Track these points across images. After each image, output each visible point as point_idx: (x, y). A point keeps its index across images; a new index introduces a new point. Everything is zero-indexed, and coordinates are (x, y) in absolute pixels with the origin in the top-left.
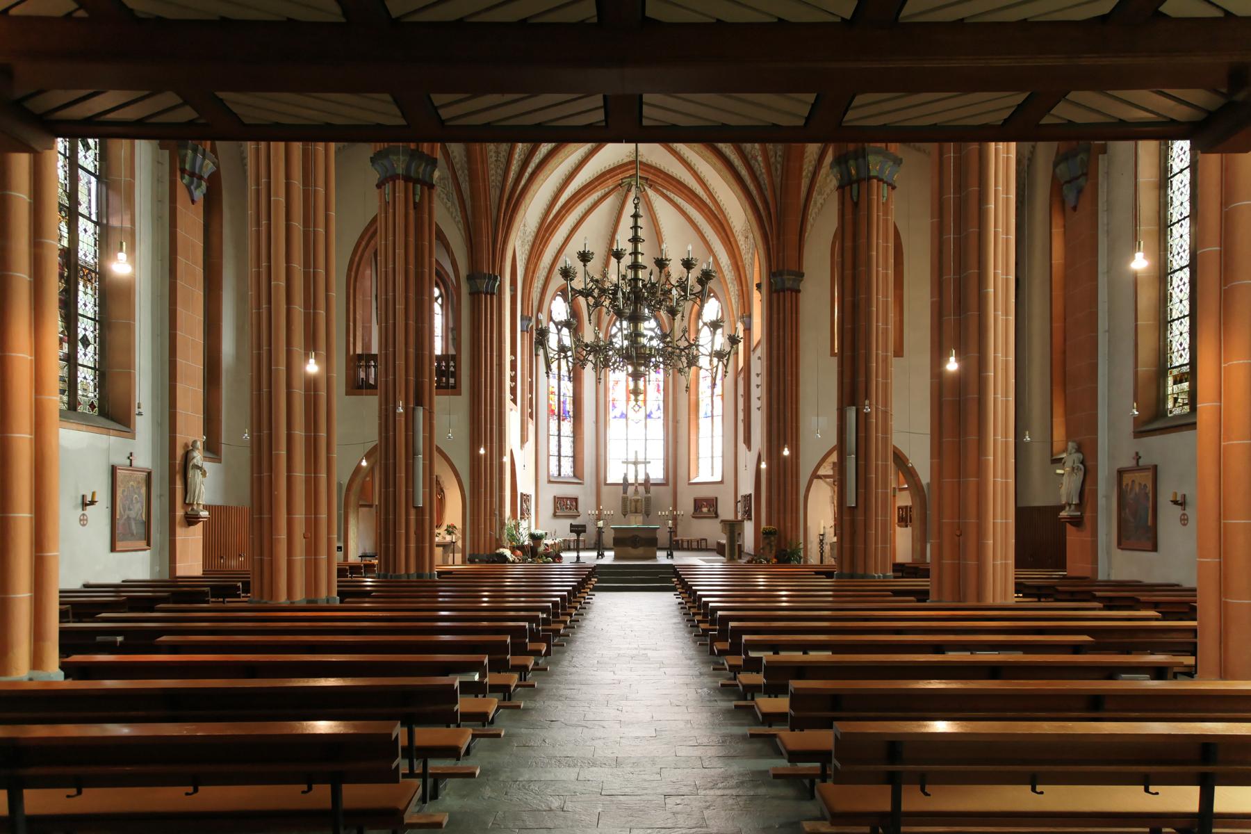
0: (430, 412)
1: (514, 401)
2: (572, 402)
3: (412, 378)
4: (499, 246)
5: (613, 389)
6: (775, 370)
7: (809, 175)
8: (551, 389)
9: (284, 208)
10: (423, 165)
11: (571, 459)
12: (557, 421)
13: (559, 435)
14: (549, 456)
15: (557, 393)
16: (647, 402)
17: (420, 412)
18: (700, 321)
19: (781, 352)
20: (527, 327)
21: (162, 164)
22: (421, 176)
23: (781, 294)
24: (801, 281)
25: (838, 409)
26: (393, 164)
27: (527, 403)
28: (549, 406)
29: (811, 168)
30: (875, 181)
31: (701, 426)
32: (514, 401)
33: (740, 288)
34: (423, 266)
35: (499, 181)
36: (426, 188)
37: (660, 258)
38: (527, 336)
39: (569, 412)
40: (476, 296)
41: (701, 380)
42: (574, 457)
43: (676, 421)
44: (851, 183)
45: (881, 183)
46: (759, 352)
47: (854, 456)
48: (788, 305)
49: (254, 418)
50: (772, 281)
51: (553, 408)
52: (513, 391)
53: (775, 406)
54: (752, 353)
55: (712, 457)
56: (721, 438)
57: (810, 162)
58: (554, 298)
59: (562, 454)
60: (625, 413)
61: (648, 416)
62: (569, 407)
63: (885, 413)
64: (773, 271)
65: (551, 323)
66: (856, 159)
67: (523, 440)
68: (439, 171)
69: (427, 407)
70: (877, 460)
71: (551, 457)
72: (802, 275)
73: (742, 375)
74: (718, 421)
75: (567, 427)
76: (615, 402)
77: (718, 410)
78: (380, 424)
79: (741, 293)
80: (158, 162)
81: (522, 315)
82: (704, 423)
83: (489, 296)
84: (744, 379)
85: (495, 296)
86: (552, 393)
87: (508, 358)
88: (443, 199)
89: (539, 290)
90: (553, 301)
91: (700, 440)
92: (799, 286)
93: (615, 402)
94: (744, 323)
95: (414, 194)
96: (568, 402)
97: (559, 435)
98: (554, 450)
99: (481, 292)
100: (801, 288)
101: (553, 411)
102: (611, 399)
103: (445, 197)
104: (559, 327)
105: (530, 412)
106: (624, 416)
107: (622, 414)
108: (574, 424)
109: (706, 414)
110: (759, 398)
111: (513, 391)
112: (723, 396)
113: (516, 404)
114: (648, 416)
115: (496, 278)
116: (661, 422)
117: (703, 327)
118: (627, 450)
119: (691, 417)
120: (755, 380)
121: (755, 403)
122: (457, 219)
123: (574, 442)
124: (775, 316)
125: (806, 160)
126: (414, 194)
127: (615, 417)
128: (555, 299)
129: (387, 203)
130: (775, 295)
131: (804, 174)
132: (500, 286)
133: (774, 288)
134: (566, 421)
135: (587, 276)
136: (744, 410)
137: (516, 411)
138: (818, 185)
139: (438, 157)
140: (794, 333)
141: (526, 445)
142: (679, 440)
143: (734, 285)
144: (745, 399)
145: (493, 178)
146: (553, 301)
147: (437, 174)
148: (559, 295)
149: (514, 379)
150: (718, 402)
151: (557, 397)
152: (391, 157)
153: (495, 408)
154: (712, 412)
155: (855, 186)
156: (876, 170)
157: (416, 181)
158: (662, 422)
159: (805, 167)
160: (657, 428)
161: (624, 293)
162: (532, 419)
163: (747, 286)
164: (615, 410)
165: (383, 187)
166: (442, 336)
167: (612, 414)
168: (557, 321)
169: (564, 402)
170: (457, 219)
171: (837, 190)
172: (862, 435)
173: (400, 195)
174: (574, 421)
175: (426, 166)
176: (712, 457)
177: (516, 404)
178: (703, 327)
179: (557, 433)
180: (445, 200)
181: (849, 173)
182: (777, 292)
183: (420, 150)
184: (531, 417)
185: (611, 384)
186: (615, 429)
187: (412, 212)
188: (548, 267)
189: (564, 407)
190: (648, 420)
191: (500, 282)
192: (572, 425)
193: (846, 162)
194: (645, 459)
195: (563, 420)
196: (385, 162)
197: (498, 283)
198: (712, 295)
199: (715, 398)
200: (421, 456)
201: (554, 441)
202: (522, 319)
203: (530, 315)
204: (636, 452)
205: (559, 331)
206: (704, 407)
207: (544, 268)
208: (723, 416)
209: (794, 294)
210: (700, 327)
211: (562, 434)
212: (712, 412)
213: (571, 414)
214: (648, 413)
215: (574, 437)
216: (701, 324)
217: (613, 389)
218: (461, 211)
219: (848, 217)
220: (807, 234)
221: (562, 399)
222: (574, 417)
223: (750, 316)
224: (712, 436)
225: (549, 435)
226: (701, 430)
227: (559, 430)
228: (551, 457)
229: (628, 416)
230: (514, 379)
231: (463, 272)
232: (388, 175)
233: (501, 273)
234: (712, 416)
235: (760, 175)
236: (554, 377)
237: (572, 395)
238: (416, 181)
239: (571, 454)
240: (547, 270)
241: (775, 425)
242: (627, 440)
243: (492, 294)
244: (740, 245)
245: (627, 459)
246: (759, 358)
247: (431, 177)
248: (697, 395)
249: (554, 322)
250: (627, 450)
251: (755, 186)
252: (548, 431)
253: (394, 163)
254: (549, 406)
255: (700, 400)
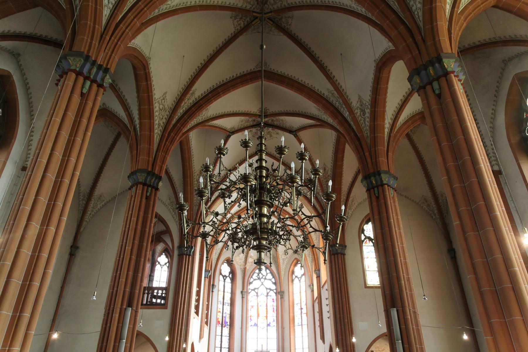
0: (136, 311)
1: (197, 313)
2: (229, 317)
3: (128, 290)
4: (195, 232)
5: (251, 310)
6: (336, 296)
7: (344, 201)
8: (219, 310)
9: (44, 166)
10: (154, 179)
11: (227, 349)
12: (221, 327)
13: (222, 336)
14: (215, 347)
15: (222, 312)
16: (268, 318)
17: (129, 311)
18: (294, 275)
19: (339, 285)
20: (208, 275)
21: (20, 177)
22: (152, 184)
23: (336, 255)
24: (345, 249)
25: (384, 310)
26: (138, 178)
27: (204, 316)
28: (217, 319)
29: (345, 198)
30: (386, 186)
31: (296, 330)
32: (197, 313)
33: (313, 256)
34: (145, 228)
35: (198, 203)
36: (154, 190)
37: (280, 145)
38: (207, 280)
39: (227, 322)
40: (181, 256)
41: (295, 305)
42: (229, 348)
43: (283, 328)
44: (373, 188)
45: (389, 187)
46: (326, 287)
47: (400, 341)
48: (340, 261)
49: (102, 336)
50: (331, 249)
51: (219, 320)
52: (197, 307)
53: (338, 316)
54: (321, 289)
55: (303, 348)
56: (307, 337)
57: (344, 195)
58: (223, 264)
59: (222, 347)
60: (256, 323)
61: (268, 325)
62: (228, 320)
63: (415, 312)
64: (331, 244)
65: (221, 276)
66: (375, 176)
67: (201, 337)
68: (162, 182)
69: (134, 308)
70: (416, 344)
71: (216, 348)
72: (346, 246)
73: (317, 301)
74: (305, 327)
75: (226, 331)
76: (251, 317)
77: (305, 322)
78: (104, 319)
79: (314, 259)
80: (18, 176)
81: (205, 269)
82: (298, 329)
83: (188, 256)
84: (318, 303)
85: (191, 256)
86: (219, 312)
87: (195, 289)
88: (171, 211)
89: (216, 259)
90: (222, 265)
91: (296, 339)
92: (344, 252)
93: (251, 317)
94: (316, 274)
95: (147, 192)
96: (227, 317)
97: (222, 336)
98: (218, 344)
99: (185, 254)
100: (346, 253)
101: (219, 322)
102: (249, 316)
103: (172, 210)
104: (225, 278)
105: (206, 321)
106: (256, 325)
107: (255, 324)
108: (230, 329)
109: (298, 324)
110: (328, 312)
111: (197, 307)
112: (307, 314)
113: (198, 315)
114: (268, 325)
115: (192, 248)
116: (275, 328)
117: (295, 278)
118: (257, 344)
119: (291, 325)
120: (325, 302)
121: (326, 315)
122: (176, 220)
123: (229, 340)
124: (334, 267)
125: (342, 194)
126: (147, 192)
127: (251, 326)
128: (223, 264)
129: (132, 196)
130: (333, 256)
131: (342, 200)
132: (194, 252)
133: (332, 253)
134: (225, 327)
135: (221, 165)
136: (319, 320)
137: (198, 319)
138: (348, 205)
139: (163, 176)
140: (344, 276)
141: (202, 340)
142: (285, 338)
143: (310, 257)
144: (319, 314)
145: (195, 201)
146: (222, 265)
147: (161, 184)
148: (225, 262)
149: (198, 301)
150: (304, 316)
151: (221, 314)
152: (137, 174)
153: (185, 316)
154: (302, 322)
155: (376, 189)
156: (386, 180)
157: (149, 186)
158: (276, 328)
159: (342, 197)
160: (273, 331)
161: (251, 186)
162: (207, 325)
163: (317, 255)
164: (252, 321)
165: (131, 189)
166: (166, 282)
167: (250, 323)
168: (223, 275)
169: (225, 317)
170: (176, 220)
171: (366, 192)
172: (403, 327)
173: (139, 192)
174: (230, 327)
175: (155, 180)
176: (303, 348)
177: (198, 315)
178: (295, 278)
179: (220, 334)
180: (172, 212)
181: (371, 182)
182: (334, 254)
183: (153, 172)
184: (207, 323)
185: (249, 308)
186: (251, 332)
187: (144, 200)
188: (221, 248)
189: (225, 320)
190: (269, 327)
191: (194, 249)
192: (229, 330)
193: (370, 178)
194: (267, 349)
195: (224, 327)
196: (135, 177)
197: (193, 250)
198: (299, 262)
199: (303, 315)
200: (125, 341)
201: (218, 338)
202: (206, 271)
203: (210, 269)
204: (262, 345)
205: (225, 280)
206: (297, 320)
207: (219, 249)
208: (307, 325)
209: (342, 255)
210: (294, 278)
211: (223, 335)
212: (302, 322)
213: (229, 323)
214: (268, 324)
215: (229, 337)
216: (294, 277)
217: (251, 310)
218: (178, 216)
219: (375, 204)
220: (346, 227)
221: (224, 316)
222: (230, 325)
223: (319, 270)
224: (302, 336)
225: (216, 335)
226: (296, 333)
227: (222, 333)
228: (216, 348)
229: (258, 325)
230: (198, 301)
231: (176, 244)
232: (135, 182)
233: (195, 246)
234: (302, 325)
235: (321, 201)
236: (221, 304)
237: (229, 313)
238: (149, 186)
239: (228, 347)
240: (220, 250)
241: (339, 326)
242: (257, 338)
243: (189, 255)
244: (312, 236)
245: (257, 350)
246: (327, 290)
247: (158, 185)
248: (294, 313)
249: (222, 275)
250: (257, 344)
251: (319, 205)
252: (216, 333)
253: (139, 177)
254: (217, 319)
255: (295, 316)
